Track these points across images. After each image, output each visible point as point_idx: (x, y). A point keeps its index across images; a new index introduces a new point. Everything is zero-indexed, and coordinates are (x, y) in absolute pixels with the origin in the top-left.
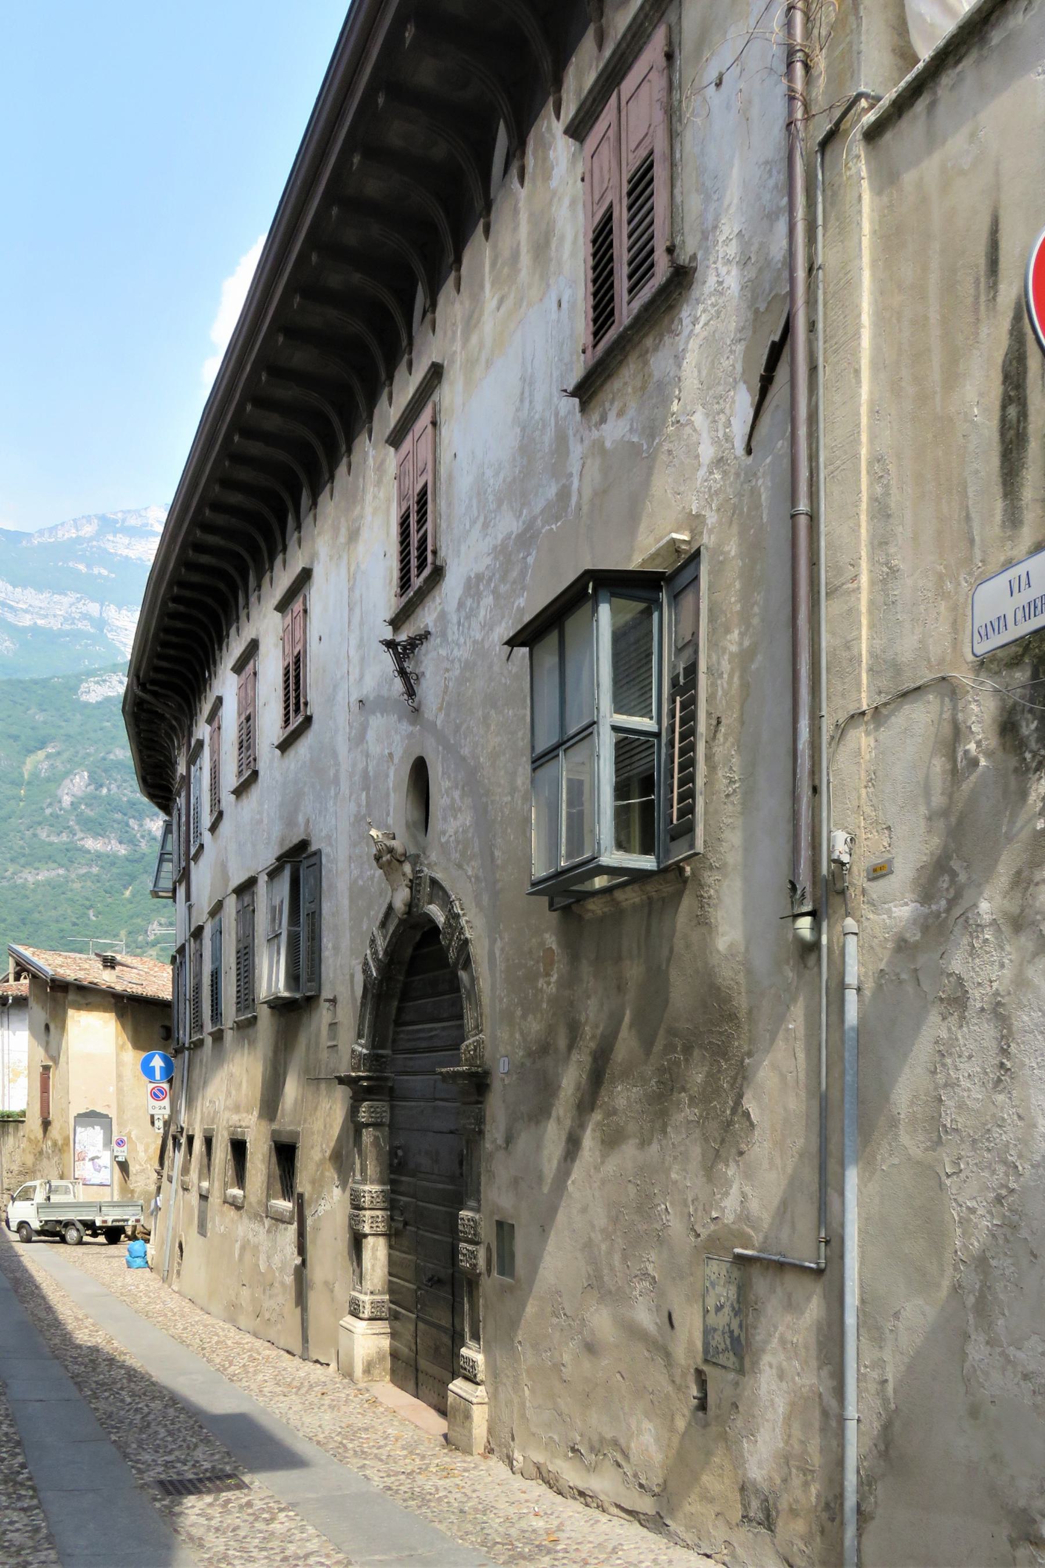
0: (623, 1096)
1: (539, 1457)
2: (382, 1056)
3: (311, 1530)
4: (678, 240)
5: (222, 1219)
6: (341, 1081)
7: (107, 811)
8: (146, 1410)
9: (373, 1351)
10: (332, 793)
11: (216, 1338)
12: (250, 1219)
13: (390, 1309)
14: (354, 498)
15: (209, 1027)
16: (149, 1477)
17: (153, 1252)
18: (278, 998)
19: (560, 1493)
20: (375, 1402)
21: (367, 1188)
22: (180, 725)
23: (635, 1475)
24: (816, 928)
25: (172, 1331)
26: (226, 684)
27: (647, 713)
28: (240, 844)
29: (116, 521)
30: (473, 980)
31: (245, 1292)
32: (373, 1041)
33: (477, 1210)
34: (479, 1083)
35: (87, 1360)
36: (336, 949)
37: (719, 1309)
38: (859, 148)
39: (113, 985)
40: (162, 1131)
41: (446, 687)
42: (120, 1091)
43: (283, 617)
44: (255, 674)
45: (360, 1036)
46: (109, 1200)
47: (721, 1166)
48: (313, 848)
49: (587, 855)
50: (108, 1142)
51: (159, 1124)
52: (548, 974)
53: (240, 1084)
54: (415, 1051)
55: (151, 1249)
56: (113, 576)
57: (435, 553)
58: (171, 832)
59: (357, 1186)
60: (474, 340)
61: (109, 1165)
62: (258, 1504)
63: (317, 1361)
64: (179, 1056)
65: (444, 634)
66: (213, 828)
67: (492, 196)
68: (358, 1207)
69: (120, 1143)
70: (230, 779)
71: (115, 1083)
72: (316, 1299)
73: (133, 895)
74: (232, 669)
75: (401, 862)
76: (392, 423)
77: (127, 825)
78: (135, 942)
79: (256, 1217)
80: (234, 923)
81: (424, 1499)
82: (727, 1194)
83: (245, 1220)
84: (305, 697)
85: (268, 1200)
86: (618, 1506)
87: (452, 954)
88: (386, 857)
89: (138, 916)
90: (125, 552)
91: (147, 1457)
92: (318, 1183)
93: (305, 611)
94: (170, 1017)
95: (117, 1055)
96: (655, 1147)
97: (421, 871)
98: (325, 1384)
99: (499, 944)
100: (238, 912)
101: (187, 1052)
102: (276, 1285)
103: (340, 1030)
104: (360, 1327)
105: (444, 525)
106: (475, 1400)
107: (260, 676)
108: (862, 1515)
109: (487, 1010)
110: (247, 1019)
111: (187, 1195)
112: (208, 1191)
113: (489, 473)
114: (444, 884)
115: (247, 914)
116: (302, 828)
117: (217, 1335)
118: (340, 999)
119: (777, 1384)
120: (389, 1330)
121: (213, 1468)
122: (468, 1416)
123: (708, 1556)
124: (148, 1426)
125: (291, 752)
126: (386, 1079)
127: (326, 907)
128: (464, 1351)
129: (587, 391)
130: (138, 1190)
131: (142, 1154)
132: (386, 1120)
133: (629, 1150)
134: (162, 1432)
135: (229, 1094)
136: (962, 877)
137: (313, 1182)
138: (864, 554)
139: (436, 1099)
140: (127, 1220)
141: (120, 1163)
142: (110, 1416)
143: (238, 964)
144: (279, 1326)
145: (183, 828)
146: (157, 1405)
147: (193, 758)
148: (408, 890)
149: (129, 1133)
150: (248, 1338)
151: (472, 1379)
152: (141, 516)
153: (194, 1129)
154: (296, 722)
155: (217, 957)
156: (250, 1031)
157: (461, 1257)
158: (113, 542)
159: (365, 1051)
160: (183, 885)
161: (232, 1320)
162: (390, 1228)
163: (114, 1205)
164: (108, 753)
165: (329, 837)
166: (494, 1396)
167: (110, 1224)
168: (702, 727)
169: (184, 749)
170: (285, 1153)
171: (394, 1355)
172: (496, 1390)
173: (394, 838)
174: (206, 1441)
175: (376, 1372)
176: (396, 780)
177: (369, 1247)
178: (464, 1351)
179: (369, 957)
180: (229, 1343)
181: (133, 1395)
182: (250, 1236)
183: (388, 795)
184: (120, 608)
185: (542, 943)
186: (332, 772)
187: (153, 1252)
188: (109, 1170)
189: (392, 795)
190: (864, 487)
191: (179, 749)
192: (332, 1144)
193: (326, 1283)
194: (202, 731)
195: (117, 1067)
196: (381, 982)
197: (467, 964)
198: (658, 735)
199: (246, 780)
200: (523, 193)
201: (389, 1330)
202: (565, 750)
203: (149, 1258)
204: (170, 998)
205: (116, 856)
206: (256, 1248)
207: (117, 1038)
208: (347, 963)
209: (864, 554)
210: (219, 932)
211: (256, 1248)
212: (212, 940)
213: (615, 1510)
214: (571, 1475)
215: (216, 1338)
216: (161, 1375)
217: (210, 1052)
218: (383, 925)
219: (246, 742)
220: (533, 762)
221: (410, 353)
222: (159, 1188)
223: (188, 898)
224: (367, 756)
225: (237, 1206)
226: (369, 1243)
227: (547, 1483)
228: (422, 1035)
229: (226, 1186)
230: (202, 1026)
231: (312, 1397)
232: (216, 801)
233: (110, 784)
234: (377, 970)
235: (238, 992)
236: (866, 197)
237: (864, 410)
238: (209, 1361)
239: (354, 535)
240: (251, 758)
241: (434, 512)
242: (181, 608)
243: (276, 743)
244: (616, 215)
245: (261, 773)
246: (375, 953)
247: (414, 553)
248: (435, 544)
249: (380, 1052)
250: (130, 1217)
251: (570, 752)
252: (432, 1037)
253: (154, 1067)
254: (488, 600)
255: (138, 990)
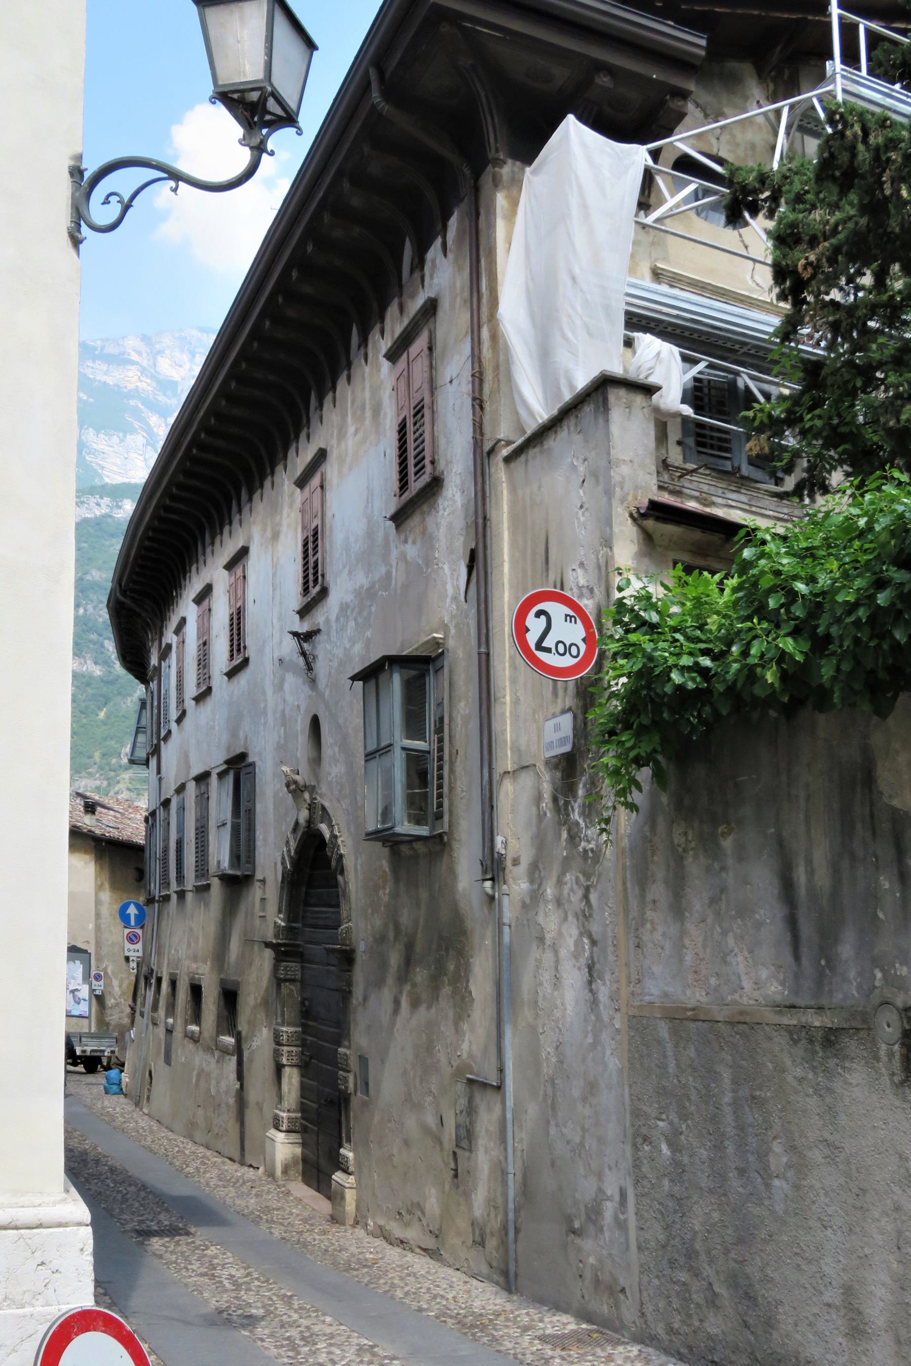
0: (420, 975)
1: (381, 1222)
2: (295, 928)
3: (229, 1254)
4: (436, 457)
5: (183, 1052)
6: (268, 945)
7: (83, 631)
8: (125, 1192)
9: (289, 1156)
10: (262, 721)
11: (177, 1149)
12: (204, 1051)
13: (301, 1124)
14: (275, 508)
15: (174, 886)
16: (129, 1227)
17: (127, 1080)
18: (225, 875)
19: (391, 1244)
20: (288, 1193)
21: (284, 1029)
22: (153, 623)
23: (428, 1225)
24: (493, 888)
25: (143, 1143)
26: (186, 608)
27: (423, 739)
28: (197, 744)
29: (95, 349)
30: (346, 883)
31: (200, 1112)
32: (289, 917)
33: (349, 1048)
34: (347, 958)
35: (79, 1160)
36: (265, 840)
37: (461, 1112)
38: (501, 465)
39: (93, 829)
40: (135, 971)
41: (330, 672)
42: (98, 928)
43: (231, 575)
44: (210, 610)
45: (280, 912)
46: (87, 1031)
47: (461, 1023)
48: (250, 759)
49: (389, 825)
50: (87, 977)
51: (133, 965)
52: (384, 888)
53: (198, 938)
54: (316, 926)
55: (125, 1078)
56: (92, 400)
57: (323, 576)
58: (145, 708)
59: (277, 1027)
60: (343, 446)
61: (87, 998)
62: (198, 1242)
63: (251, 1166)
64: (151, 905)
65: (329, 635)
66: (179, 721)
67: (352, 358)
68: (278, 1043)
69: (98, 977)
70: (191, 689)
71: (93, 919)
72: (251, 1116)
73: (108, 716)
74: (193, 601)
75: (302, 791)
76: (299, 473)
77: (103, 646)
78: (109, 764)
79: (208, 1049)
80: (193, 804)
81: (305, 1245)
82: (463, 1041)
83: (201, 1052)
84: (244, 642)
85: (218, 1036)
86: (420, 1247)
87: (333, 863)
88: (293, 787)
89: (112, 738)
90: (104, 378)
91: (125, 1217)
92: (252, 1023)
93: (244, 577)
94: (142, 860)
95: (96, 894)
96: (433, 1010)
97: (315, 799)
98: (254, 1181)
99: (359, 861)
100: (197, 797)
101: (157, 905)
102: (223, 1105)
103: (266, 908)
104: (280, 1137)
105: (328, 560)
106: (347, 1185)
107: (213, 612)
108: (517, 1231)
109: (353, 906)
110: (203, 885)
111: (157, 1030)
112: (173, 1026)
113: (352, 539)
114: (329, 811)
115: (203, 799)
116: (242, 742)
117: (178, 1146)
118: (268, 881)
119: (483, 1158)
120: (300, 1141)
121: (171, 1225)
122: (343, 1198)
123: (458, 1270)
124: (127, 1200)
125: (235, 680)
126: (298, 946)
127: (259, 807)
128: (342, 1151)
129: (399, 518)
130: (113, 1023)
131: (117, 989)
132: (298, 977)
133: (422, 1009)
134: (137, 1205)
135: (189, 944)
136: (542, 874)
137: (249, 1023)
138: (507, 684)
139: (329, 965)
140: (103, 1051)
141: (97, 996)
142: (100, 1193)
143: (196, 838)
144: (225, 1139)
145: (155, 711)
146: (132, 1189)
147: (165, 653)
148: (307, 811)
149: (106, 968)
150: (202, 1149)
151: (346, 1171)
152: (118, 345)
153: (162, 972)
154: (238, 661)
155: (181, 829)
156: (206, 895)
157: (339, 1082)
158: (93, 368)
159: (283, 924)
160: (155, 758)
161: (190, 1137)
162: (301, 1060)
163: (92, 1036)
164: (86, 573)
165: (260, 754)
166: (358, 1182)
167: (88, 1054)
168: (446, 757)
169: (156, 644)
170: (230, 998)
171: (305, 1160)
172: (360, 1178)
173: (298, 774)
174: (167, 1210)
175: (291, 1173)
176: (302, 725)
177: (287, 1075)
178: (342, 1151)
179: (285, 853)
180: (187, 1152)
181: (115, 1182)
182: (204, 1065)
183: (297, 736)
184: (98, 432)
185: (381, 866)
186: (262, 705)
187: (127, 1080)
188: (87, 1003)
189: (300, 737)
190: (507, 648)
191: (153, 641)
192: (262, 993)
193: (258, 1104)
194: (170, 637)
195: (96, 907)
196: (293, 874)
197: (342, 872)
198: (429, 752)
199: (203, 693)
200: (367, 369)
201: (300, 1141)
202: (380, 755)
203: (123, 1087)
204: (142, 842)
205: (91, 677)
206: (208, 1075)
207: (96, 879)
208: (272, 855)
209: (507, 684)
210: (182, 808)
211: (208, 1075)
212: (177, 813)
213: (418, 1250)
214: (397, 1231)
215: (177, 1149)
216: (136, 1172)
217: (175, 907)
218: (295, 830)
219: (203, 662)
220: (366, 756)
221: (308, 428)
222: (133, 1022)
223: (159, 771)
224: (285, 701)
225: (194, 1039)
226: (287, 1071)
227: (385, 1238)
228: (320, 915)
229: (186, 1023)
230: (169, 884)
231: (245, 1189)
232: (181, 701)
233: (86, 604)
234: (291, 863)
235: (197, 862)
236: (505, 492)
237: (506, 606)
238: (171, 1164)
239: (276, 536)
240: (207, 676)
241: (323, 547)
242: (155, 545)
243: (225, 671)
244: (408, 425)
245: (214, 690)
246: (289, 851)
247: (311, 571)
248: (323, 571)
249: (294, 925)
250: (106, 1048)
251: (383, 757)
252: (326, 918)
253: (129, 914)
254: (352, 624)
255: (114, 834)
